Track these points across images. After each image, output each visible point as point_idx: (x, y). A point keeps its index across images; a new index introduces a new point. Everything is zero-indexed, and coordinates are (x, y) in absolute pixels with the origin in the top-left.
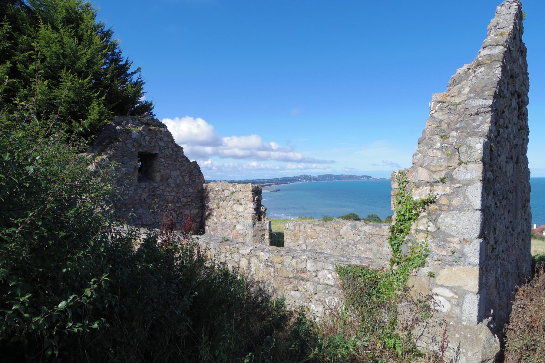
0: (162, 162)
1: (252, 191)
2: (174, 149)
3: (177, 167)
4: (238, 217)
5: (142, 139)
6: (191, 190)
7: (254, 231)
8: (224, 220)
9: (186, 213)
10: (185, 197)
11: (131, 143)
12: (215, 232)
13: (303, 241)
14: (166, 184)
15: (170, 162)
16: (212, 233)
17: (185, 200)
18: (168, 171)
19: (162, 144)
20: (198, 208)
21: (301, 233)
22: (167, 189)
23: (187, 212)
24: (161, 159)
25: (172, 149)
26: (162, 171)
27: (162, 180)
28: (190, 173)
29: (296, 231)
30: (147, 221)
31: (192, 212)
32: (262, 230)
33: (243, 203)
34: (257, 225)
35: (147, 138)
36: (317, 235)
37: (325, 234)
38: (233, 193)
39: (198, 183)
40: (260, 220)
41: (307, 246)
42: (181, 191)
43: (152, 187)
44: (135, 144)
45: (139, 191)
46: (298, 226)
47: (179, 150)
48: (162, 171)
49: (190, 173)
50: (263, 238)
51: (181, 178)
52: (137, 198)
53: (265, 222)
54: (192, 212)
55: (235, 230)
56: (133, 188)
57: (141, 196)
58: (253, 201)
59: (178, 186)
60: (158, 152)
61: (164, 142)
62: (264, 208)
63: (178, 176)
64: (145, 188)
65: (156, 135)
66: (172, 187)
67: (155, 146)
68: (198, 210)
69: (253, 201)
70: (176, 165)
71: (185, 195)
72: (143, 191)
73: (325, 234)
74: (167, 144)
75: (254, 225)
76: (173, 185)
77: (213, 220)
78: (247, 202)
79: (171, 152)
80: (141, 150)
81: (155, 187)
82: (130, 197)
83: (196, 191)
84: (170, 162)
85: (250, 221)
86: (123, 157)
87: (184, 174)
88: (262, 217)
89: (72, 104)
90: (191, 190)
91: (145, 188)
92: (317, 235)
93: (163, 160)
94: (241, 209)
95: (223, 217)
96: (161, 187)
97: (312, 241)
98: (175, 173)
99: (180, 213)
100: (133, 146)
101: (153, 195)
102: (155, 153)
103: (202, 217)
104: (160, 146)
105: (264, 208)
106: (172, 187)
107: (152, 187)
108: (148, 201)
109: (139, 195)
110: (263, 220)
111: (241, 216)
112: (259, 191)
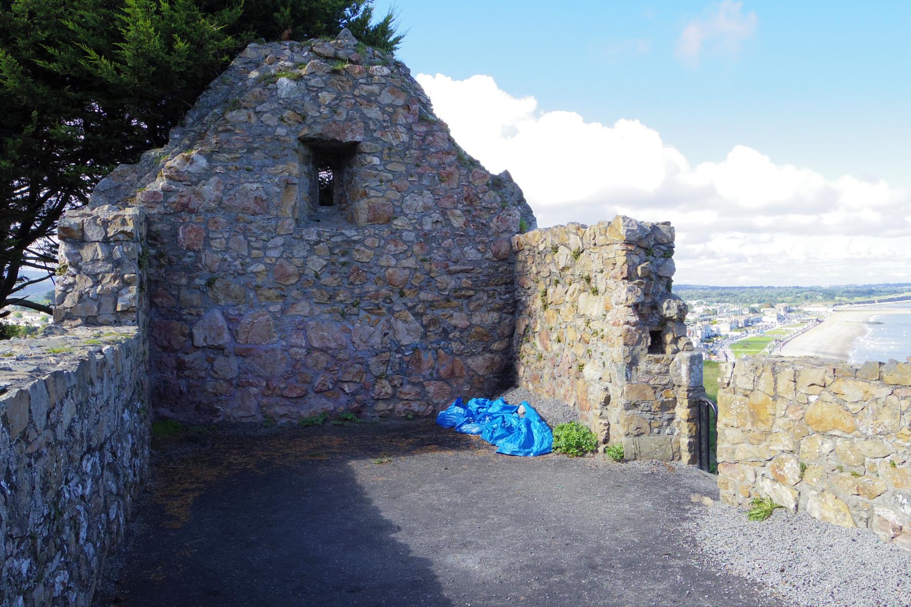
0: (374, 167)
1: (628, 242)
2: (415, 128)
3: (425, 182)
4: (591, 335)
5: (307, 99)
6: (472, 254)
7: (631, 389)
8: (556, 347)
9: (453, 322)
10: (450, 273)
11: (273, 112)
12: (537, 384)
13: (783, 442)
14: (386, 233)
15: (402, 168)
16: (531, 387)
17: (452, 284)
18: (393, 195)
19: (374, 113)
20: (499, 310)
21: (781, 406)
22: (391, 247)
23: (459, 320)
24: (369, 158)
25: (409, 129)
26: (372, 193)
27: (372, 221)
28: (470, 200)
29: (758, 398)
30: (323, 338)
31: (476, 320)
32: (665, 387)
33: (601, 288)
34: (642, 366)
35: (326, 97)
36: (848, 423)
37: (887, 420)
38: (577, 254)
39: (497, 234)
40: (657, 346)
41: (803, 468)
42: (438, 255)
43: (339, 239)
44: (287, 113)
45: (300, 251)
46: (767, 375)
47: (430, 133)
48: (372, 193)
49: (470, 200)
50: (666, 416)
51: (436, 216)
52: (291, 269)
53: (677, 357)
54: (476, 320)
55: (581, 382)
56: (279, 241)
57: (305, 264)
58: (629, 278)
59: (426, 238)
60: (358, 138)
61: (382, 109)
62: (674, 304)
63: (426, 208)
64: (317, 243)
65: (354, 87)
66: (405, 242)
67: (350, 119)
68: (495, 315)
69: (629, 278)
70: (421, 176)
71: (453, 268)
72: (312, 251)
73: (887, 420)
74: (390, 115)
75: (632, 364)
76: (410, 236)
77: (534, 346)
78: (611, 282)
79: (405, 138)
80: (305, 132)
81: (349, 242)
82: (270, 268)
83: (489, 255)
84: (402, 168)
85: (617, 351)
86: (251, 150)
87: (448, 204)
88: (669, 338)
89: (358, 100)
90: (472, 254)
91: (317, 243)
92: (848, 423)
93: (376, 161)
94: (592, 306)
95: (554, 336)
96: (368, 242)
97: (827, 446)
98: (417, 202)
99: (434, 322)
100: (282, 119)
101: (344, 264)
102: (349, 139)
103: (511, 335)
104: (366, 120)
105: (674, 304)
106: (405, 242)
107: (339, 239)
108: (326, 279)
109: (298, 262)
110: (669, 349)
111: (595, 333)
112: (658, 243)
